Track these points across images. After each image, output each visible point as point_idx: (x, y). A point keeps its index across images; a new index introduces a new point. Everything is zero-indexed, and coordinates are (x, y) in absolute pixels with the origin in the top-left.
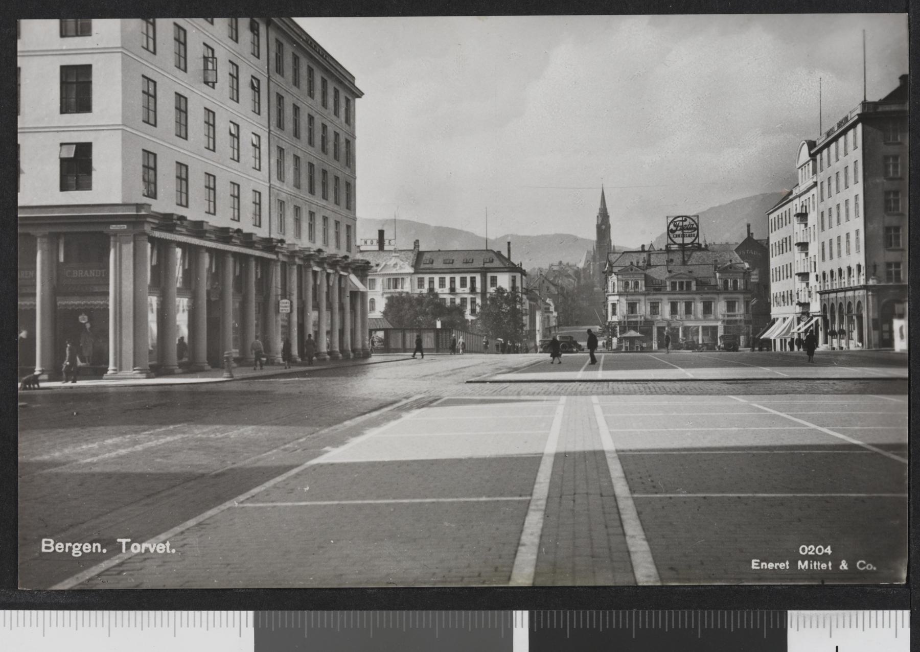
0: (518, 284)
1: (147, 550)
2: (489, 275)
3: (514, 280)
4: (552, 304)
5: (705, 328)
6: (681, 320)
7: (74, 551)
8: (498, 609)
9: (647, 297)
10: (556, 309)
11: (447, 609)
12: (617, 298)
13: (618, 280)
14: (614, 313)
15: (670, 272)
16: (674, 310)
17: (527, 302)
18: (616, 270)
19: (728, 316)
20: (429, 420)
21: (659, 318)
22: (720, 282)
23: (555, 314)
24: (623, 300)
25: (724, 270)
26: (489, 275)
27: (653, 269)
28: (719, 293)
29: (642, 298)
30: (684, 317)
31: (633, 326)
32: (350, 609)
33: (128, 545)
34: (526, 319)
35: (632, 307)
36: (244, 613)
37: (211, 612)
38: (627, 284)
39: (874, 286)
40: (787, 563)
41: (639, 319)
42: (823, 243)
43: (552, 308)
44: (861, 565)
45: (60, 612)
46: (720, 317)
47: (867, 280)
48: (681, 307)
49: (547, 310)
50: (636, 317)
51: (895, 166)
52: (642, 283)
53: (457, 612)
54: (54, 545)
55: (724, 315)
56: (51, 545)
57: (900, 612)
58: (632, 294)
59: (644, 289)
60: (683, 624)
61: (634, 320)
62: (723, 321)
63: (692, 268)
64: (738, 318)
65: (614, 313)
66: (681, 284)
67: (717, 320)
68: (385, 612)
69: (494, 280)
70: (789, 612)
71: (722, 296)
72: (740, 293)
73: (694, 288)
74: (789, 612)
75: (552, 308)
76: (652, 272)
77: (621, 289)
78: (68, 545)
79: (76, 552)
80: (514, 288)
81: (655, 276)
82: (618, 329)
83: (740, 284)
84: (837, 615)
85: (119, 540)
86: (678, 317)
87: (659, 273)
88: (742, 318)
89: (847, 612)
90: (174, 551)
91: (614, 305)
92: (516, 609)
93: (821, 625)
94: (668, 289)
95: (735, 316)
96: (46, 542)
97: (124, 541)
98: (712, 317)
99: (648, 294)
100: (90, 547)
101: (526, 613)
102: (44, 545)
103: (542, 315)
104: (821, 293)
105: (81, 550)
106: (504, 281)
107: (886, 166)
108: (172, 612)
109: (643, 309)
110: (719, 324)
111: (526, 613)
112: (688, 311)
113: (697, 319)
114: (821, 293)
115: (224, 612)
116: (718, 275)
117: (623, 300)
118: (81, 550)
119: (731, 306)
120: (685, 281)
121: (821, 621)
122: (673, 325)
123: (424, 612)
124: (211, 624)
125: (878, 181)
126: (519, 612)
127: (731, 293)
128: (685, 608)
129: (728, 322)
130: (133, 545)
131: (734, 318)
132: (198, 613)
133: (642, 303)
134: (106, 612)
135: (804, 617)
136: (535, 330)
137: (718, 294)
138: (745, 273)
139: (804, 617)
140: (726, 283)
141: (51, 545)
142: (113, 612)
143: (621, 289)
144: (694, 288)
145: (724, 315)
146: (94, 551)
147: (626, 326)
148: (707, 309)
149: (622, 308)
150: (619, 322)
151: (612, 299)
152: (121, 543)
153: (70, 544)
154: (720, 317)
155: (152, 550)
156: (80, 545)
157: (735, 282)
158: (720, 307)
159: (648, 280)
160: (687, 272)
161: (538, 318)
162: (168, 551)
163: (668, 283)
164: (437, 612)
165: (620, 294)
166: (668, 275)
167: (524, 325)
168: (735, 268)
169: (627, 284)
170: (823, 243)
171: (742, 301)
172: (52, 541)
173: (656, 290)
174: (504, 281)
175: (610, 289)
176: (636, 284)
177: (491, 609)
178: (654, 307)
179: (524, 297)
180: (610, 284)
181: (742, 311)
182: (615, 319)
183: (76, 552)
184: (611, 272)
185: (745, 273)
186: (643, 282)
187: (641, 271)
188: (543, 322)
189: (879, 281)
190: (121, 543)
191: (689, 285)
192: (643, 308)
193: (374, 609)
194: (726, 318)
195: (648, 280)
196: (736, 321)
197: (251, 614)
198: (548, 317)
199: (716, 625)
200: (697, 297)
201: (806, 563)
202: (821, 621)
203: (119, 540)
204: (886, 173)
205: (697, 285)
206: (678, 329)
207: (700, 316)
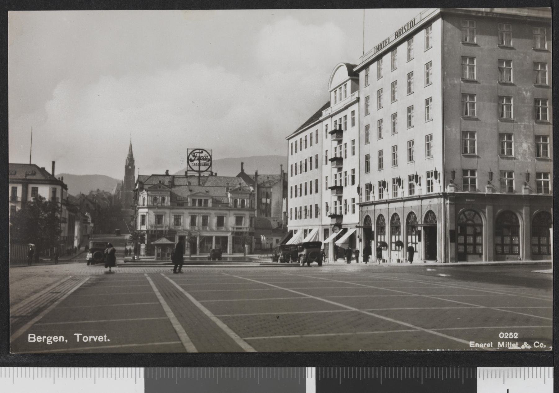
0: (58, 195)
1: (92, 339)
2: (31, 186)
3: (54, 192)
4: (89, 216)
5: (217, 238)
6: (199, 231)
7: (48, 342)
8: (296, 366)
9: (172, 211)
10: (93, 221)
11: (265, 366)
12: (146, 210)
13: (148, 195)
14: (143, 223)
15: (191, 191)
16: (193, 223)
17: (67, 212)
18: (146, 187)
19: (237, 228)
20: (271, 255)
21: (181, 228)
22: (231, 201)
23: (92, 225)
24: (152, 213)
25: (234, 192)
26: (31, 186)
27: (177, 188)
28: (230, 209)
29: (167, 211)
30: (201, 229)
31: (160, 234)
32: (204, 366)
33: (81, 337)
34: (64, 226)
35: (159, 218)
36: (138, 369)
37: (117, 368)
38: (155, 199)
39: (453, 194)
40: (492, 344)
41: (164, 229)
42: (367, 157)
43: (90, 220)
44: (537, 344)
45: (23, 368)
46: (230, 229)
47: (445, 187)
48: (199, 220)
49: (85, 221)
50: (162, 227)
51: (472, 68)
52: (167, 199)
53: (271, 368)
54: (36, 338)
55: (233, 228)
56: (34, 338)
57: (547, 368)
58: (159, 208)
59: (169, 203)
60: (412, 375)
61: (160, 229)
62: (233, 233)
63: (208, 189)
64: (244, 230)
65: (143, 223)
66: (200, 201)
67: (227, 231)
68: (226, 368)
69: (35, 190)
70: (478, 368)
71: (232, 213)
72: (247, 210)
73: (210, 204)
74: (478, 368)
75: (90, 220)
76: (175, 190)
77: (151, 204)
78: (44, 337)
79: (49, 342)
80: (54, 198)
81: (179, 194)
82: (146, 237)
83: (247, 202)
84: (508, 370)
85: (75, 334)
86: (196, 228)
87: (182, 192)
88: (248, 230)
89: (514, 368)
90: (66, 341)
91: (143, 216)
92: (308, 366)
93: (498, 376)
94: (190, 204)
95: (241, 228)
96: (33, 339)
97: (78, 335)
98: (224, 229)
99: (173, 208)
100: (57, 338)
101: (314, 369)
102: (29, 338)
103: (81, 225)
104: (361, 205)
105: (52, 340)
106: (45, 192)
107: (463, 68)
108: (93, 369)
109: (168, 221)
110: (229, 235)
111: (314, 369)
112: (205, 223)
113: (211, 230)
114: (361, 205)
115: (125, 368)
116: (229, 195)
117: (152, 213)
118: (52, 340)
119: (239, 220)
120: (203, 199)
121: (498, 374)
122: (193, 235)
123: (250, 368)
124: (117, 376)
125: (456, 82)
126: (309, 368)
127: (239, 210)
128: (413, 366)
129: (237, 233)
130: (84, 338)
131: (241, 230)
132: (109, 369)
133: (168, 215)
134: (52, 368)
135: (492, 371)
136: (73, 237)
137: (229, 210)
138: (250, 194)
139: (492, 371)
140: (236, 201)
141: (34, 338)
142: (56, 369)
143: (151, 204)
144: (210, 204)
145: (233, 228)
146: (60, 341)
147: (154, 235)
148: (220, 221)
149: (151, 219)
150: (147, 231)
151: (142, 211)
152: (76, 336)
153: (45, 337)
154: (230, 229)
155: (95, 340)
156: (51, 338)
157: (243, 202)
158: (230, 221)
159: (173, 197)
160: (204, 191)
161: (77, 228)
162: (105, 341)
163: (189, 200)
164: (258, 368)
165: (149, 207)
166: (189, 193)
167: (60, 231)
168: (243, 190)
169: (155, 199)
170: (367, 157)
171: (247, 216)
172: (34, 335)
173: (179, 205)
174: (45, 192)
175: (141, 202)
176: (163, 199)
177: (292, 366)
178: (177, 219)
179: (64, 207)
180: (141, 199)
181: (247, 225)
182: (144, 228)
183: (49, 342)
184: (141, 189)
185: (250, 194)
186: (169, 198)
187: (168, 189)
188: (81, 230)
189: (457, 189)
190: (76, 336)
191: (206, 201)
192: (168, 219)
193: (219, 366)
194: (235, 230)
195: (173, 197)
196: (242, 233)
197: (142, 369)
198: (86, 227)
199: (432, 376)
200: (213, 212)
201: (503, 343)
202: (498, 374)
203: (75, 334)
204: (463, 74)
205: (213, 203)
206: (196, 239)
207: (214, 228)
